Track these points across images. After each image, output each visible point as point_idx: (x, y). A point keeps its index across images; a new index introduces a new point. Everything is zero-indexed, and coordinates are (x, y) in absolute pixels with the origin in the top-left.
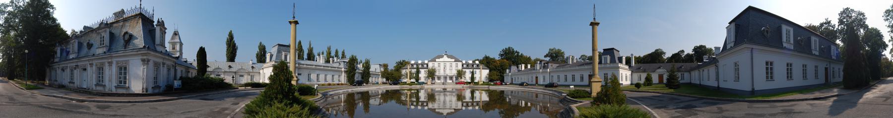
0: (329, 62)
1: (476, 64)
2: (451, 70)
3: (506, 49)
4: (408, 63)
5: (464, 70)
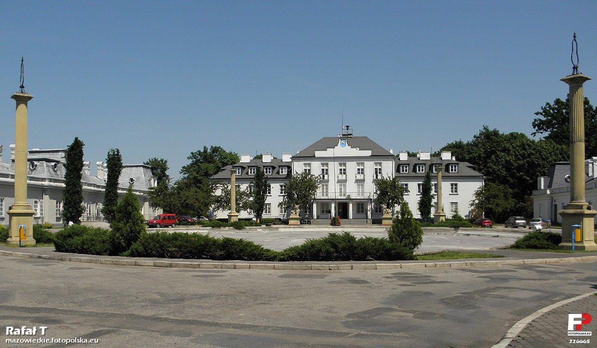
2: (360, 182)
3: (558, 102)
4: (232, 160)
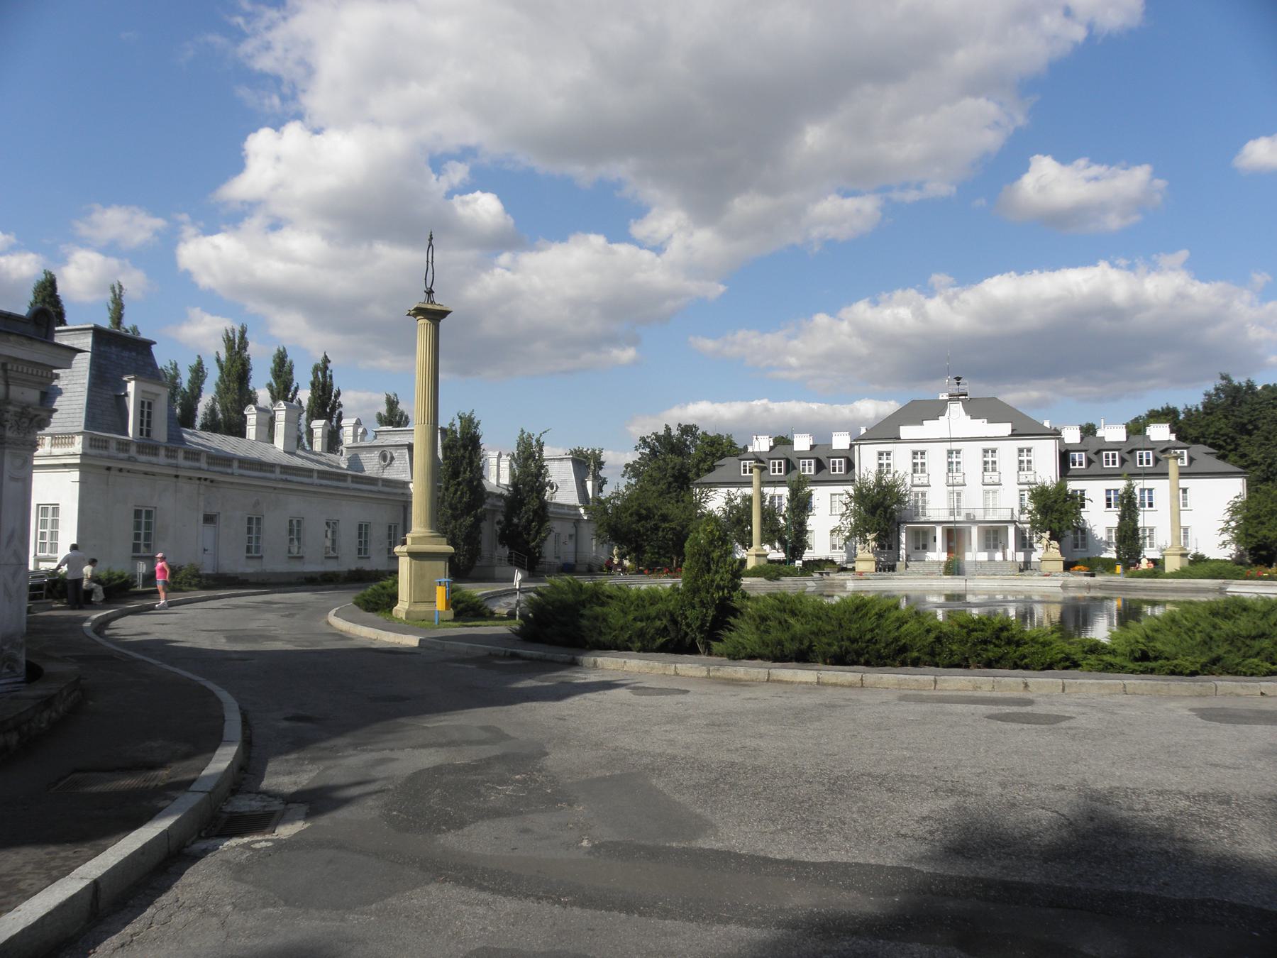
0: (241, 433)
1: (1152, 446)
5: (1072, 485)
